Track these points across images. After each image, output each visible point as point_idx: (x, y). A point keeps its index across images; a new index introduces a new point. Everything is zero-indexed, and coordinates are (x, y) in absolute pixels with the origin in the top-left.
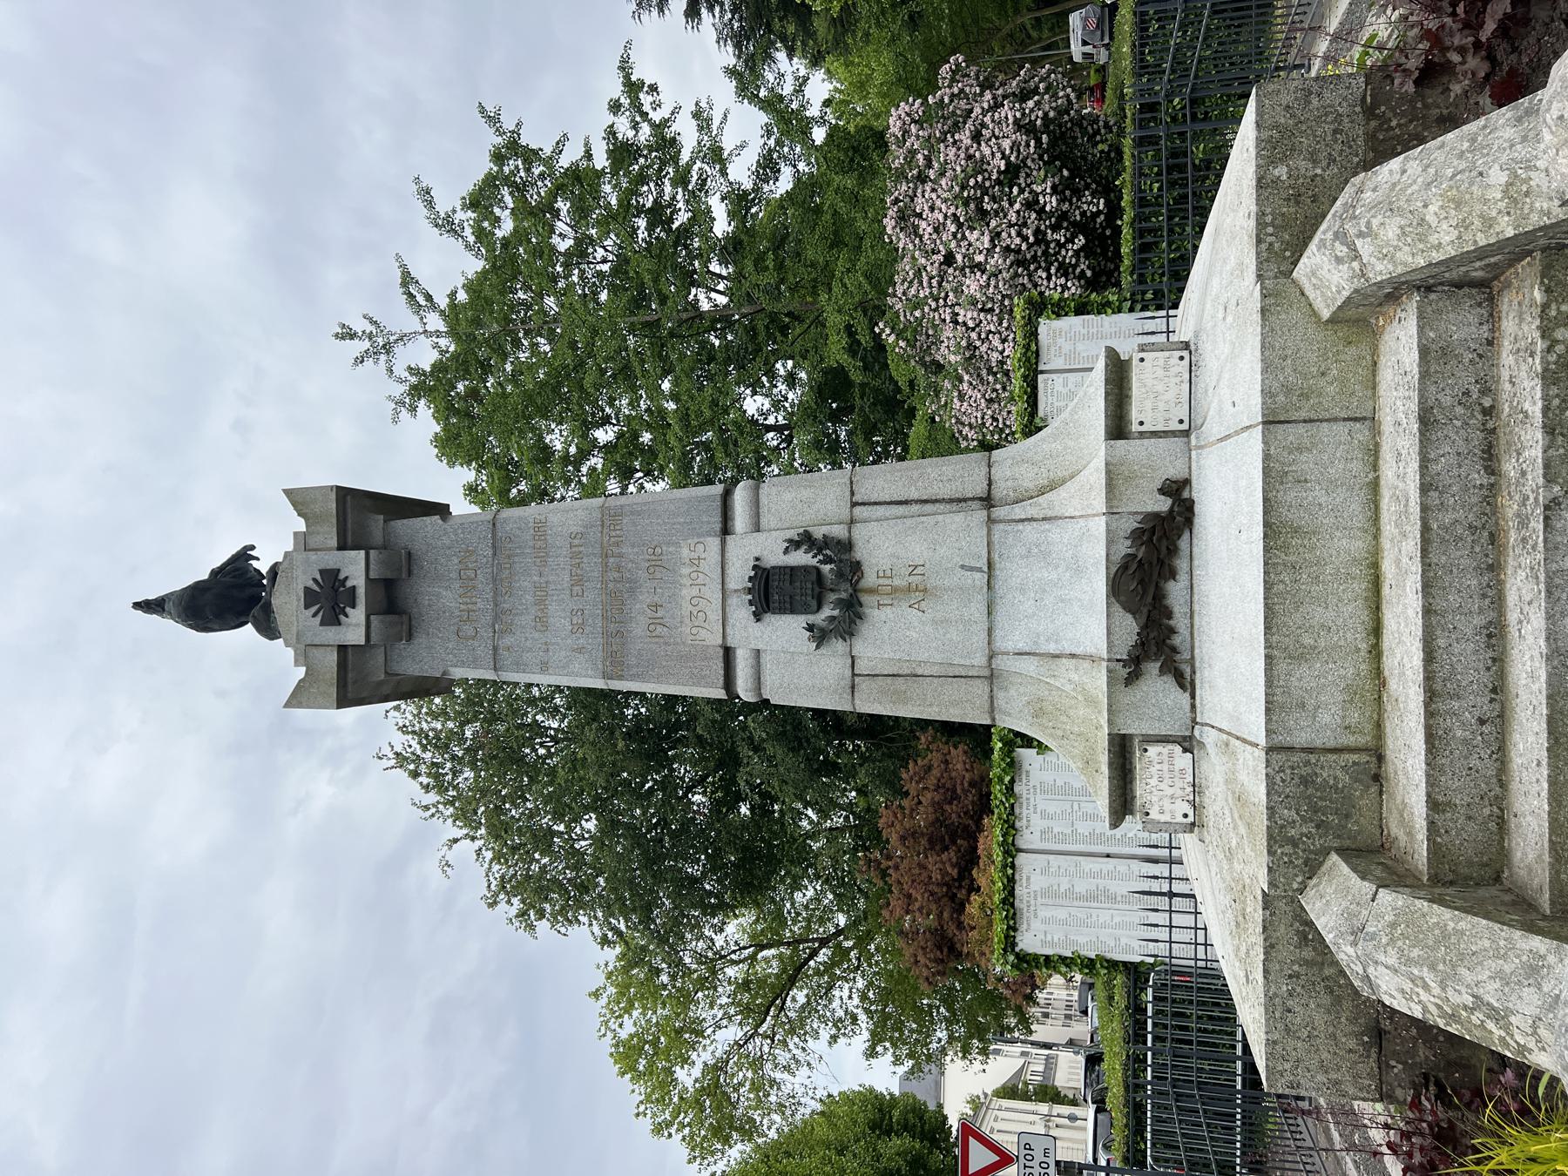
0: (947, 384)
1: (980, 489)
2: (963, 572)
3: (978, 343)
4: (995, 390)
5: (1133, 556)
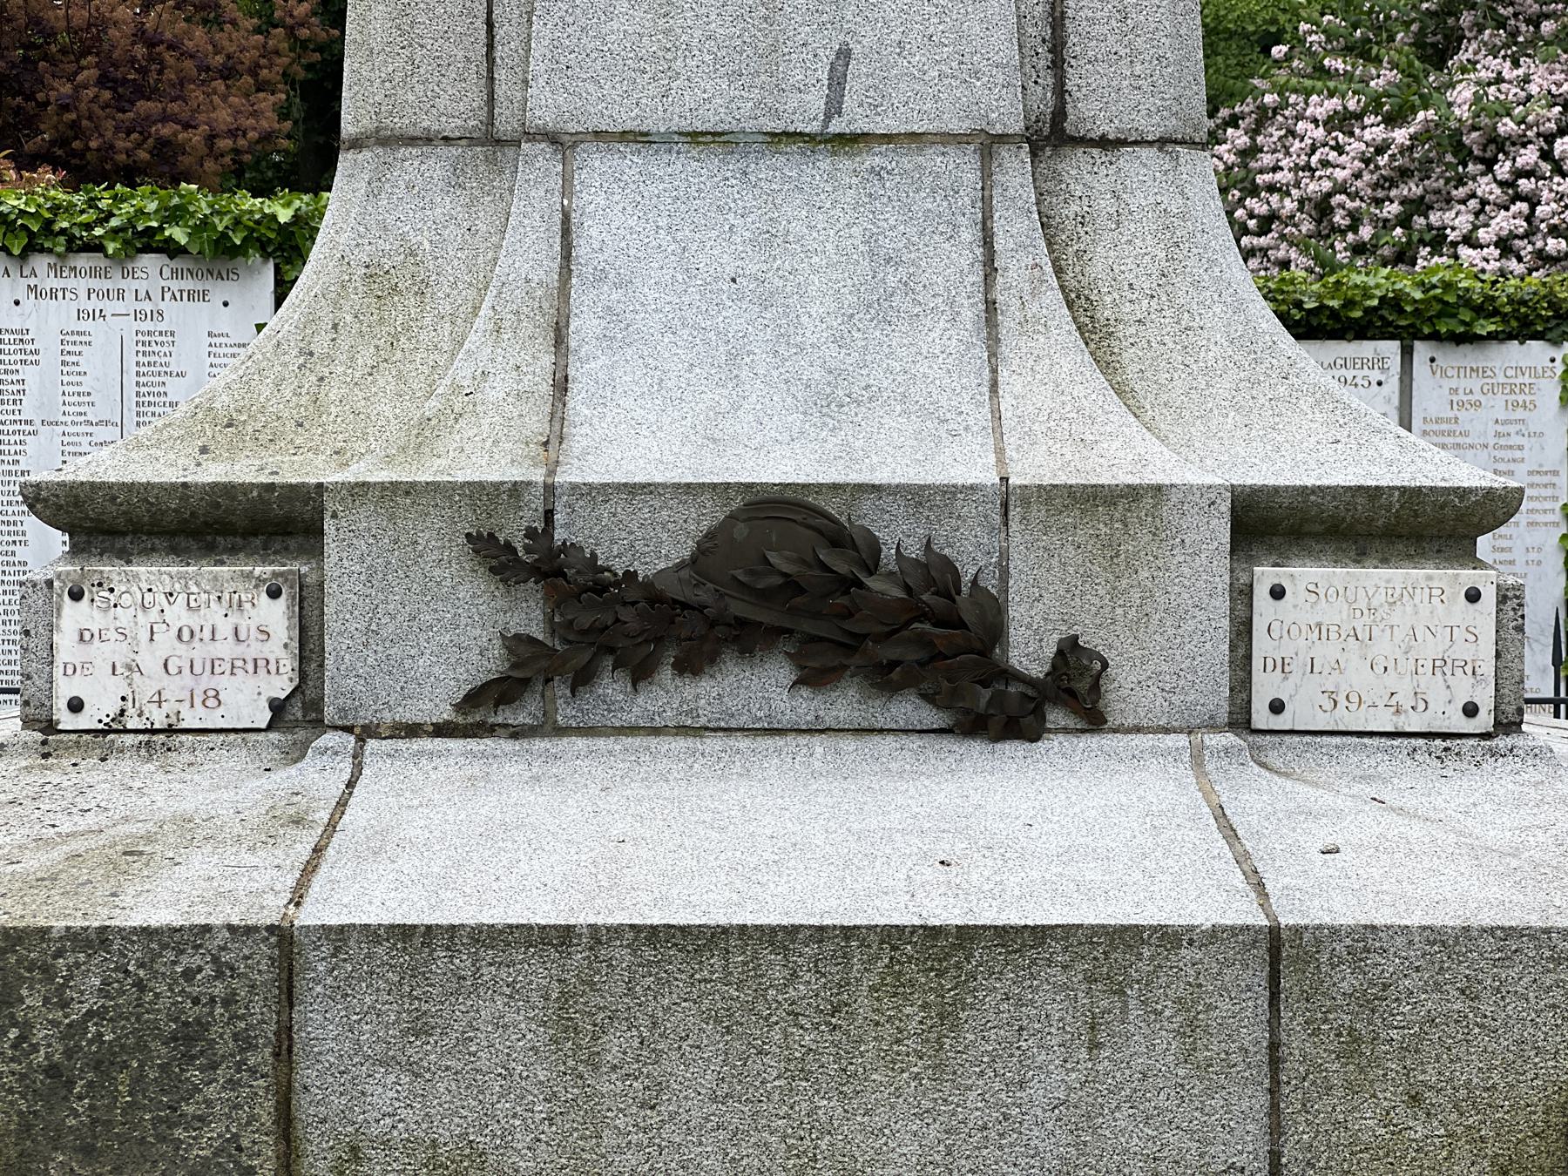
0: (1384, 78)
1: (1092, 110)
2: (827, 56)
3: (1503, 170)
4: (1355, 220)
5: (871, 563)
